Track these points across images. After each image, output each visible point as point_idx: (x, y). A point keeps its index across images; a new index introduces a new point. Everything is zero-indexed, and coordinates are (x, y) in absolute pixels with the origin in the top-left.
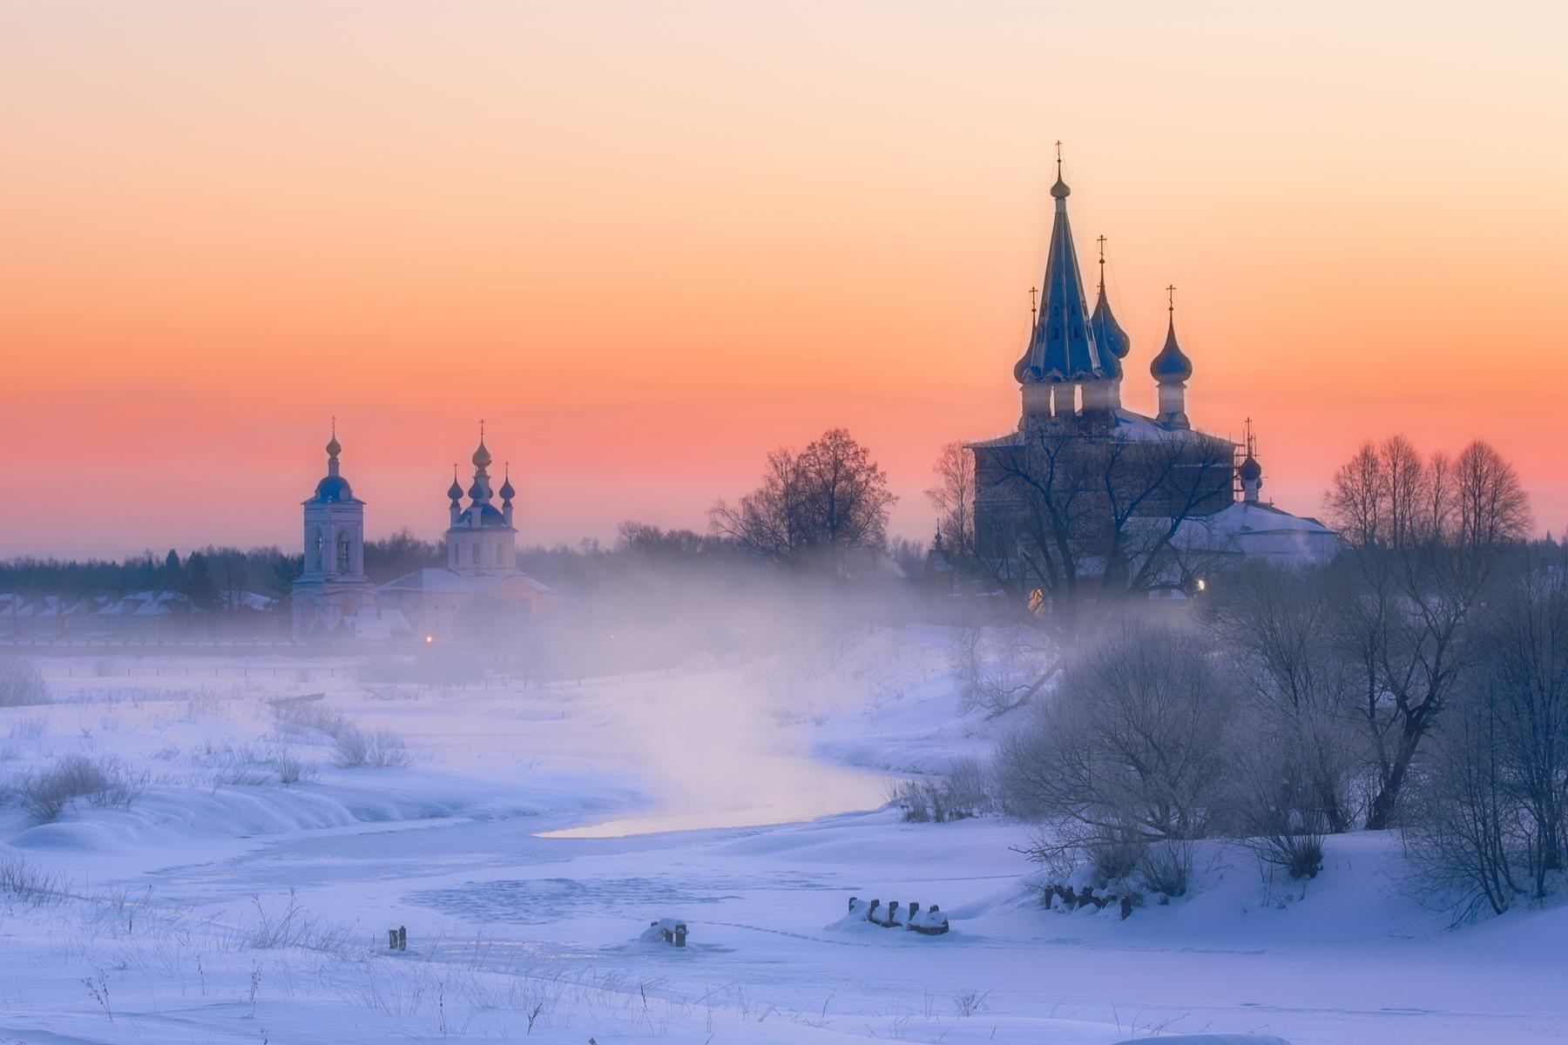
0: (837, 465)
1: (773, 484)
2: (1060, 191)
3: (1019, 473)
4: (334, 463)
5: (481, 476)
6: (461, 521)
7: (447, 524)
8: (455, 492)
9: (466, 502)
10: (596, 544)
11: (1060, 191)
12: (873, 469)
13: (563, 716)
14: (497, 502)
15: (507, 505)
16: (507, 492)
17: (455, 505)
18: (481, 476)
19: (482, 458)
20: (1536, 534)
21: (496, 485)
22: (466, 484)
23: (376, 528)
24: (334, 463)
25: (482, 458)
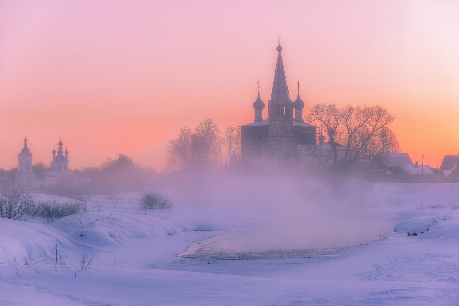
0: (209, 129)
1: (181, 137)
2: (279, 49)
3: (319, 119)
4: (26, 144)
5: (60, 148)
6: (56, 159)
7: (52, 160)
8: (54, 152)
9: (57, 154)
10: (110, 159)
11: (279, 49)
12: (218, 130)
13: (434, 207)
14: (64, 155)
15: (67, 155)
16: (67, 152)
17: (54, 155)
18: (60, 148)
19: (61, 144)
20: (402, 152)
21: (64, 150)
22: (57, 150)
23: (35, 161)
24: (26, 144)
25: (61, 144)
